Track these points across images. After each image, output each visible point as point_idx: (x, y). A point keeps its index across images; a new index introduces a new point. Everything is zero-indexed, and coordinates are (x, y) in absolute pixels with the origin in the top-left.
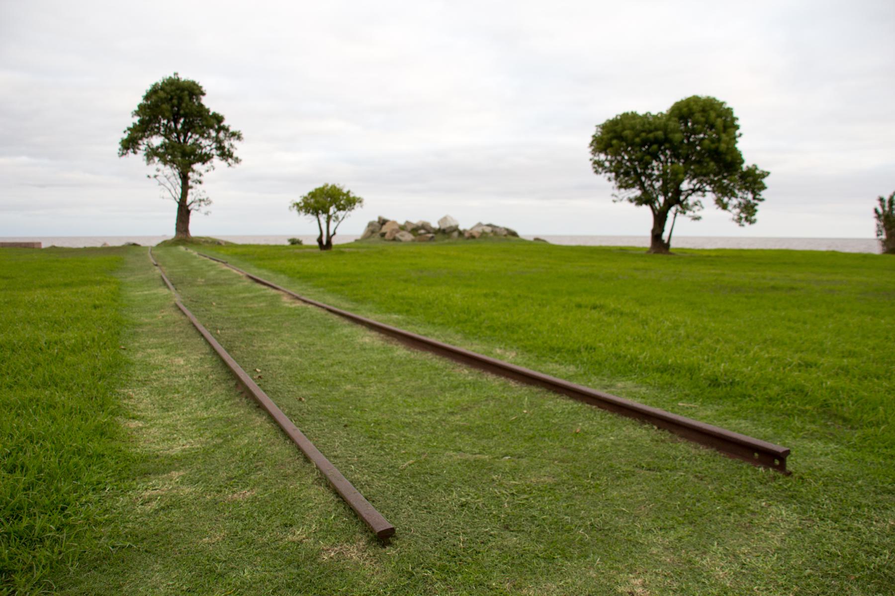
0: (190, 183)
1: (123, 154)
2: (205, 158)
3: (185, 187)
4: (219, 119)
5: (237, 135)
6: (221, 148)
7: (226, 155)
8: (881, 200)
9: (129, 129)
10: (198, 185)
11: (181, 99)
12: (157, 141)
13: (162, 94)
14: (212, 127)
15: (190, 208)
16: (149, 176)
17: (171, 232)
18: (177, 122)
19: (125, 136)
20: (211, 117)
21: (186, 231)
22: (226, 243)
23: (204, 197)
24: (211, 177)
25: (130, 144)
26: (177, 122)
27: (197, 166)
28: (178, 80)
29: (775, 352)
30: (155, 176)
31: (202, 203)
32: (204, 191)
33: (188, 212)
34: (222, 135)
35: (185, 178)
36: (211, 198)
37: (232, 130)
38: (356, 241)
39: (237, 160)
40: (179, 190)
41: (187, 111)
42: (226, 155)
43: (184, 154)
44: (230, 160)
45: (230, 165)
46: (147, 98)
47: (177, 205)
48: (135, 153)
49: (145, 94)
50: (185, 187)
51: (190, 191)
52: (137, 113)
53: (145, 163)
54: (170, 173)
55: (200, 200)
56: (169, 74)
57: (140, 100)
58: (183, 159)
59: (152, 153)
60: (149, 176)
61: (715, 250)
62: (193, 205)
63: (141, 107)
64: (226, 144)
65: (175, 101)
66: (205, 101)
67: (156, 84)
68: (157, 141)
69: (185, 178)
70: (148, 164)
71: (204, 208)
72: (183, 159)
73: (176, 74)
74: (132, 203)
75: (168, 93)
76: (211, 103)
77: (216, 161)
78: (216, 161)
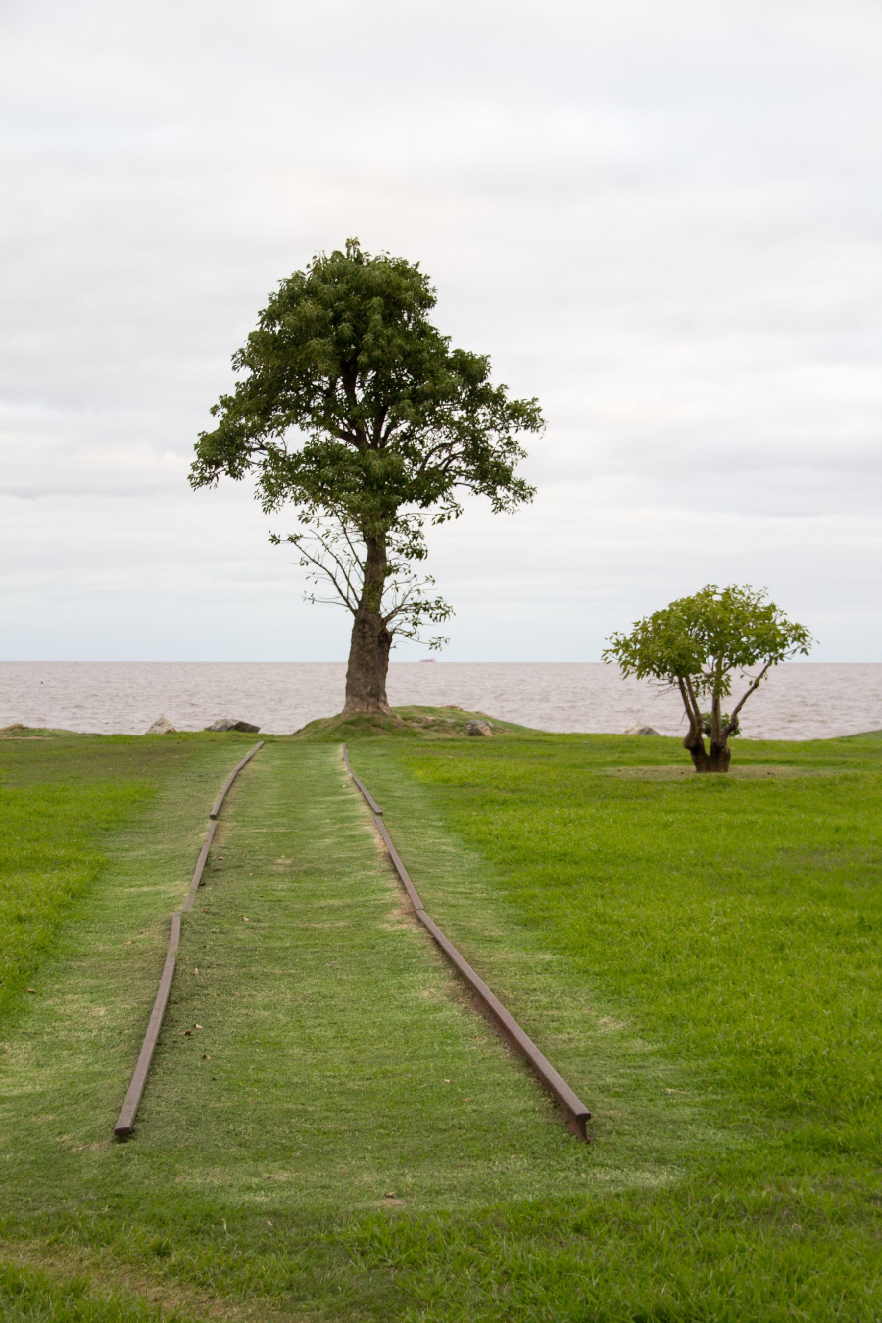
0: (391, 554)
1: (205, 480)
2: (431, 486)
3: (376, 569)
4: (471, 369)
5: (525, 415)
6: (477, 453)
7: (492, 474)
8: (729, 694)
9: (226, 402)
10: (414, 561)
11: (361, 320)
12: (295, 439)
13: (309, 307)
14: (450, 395)
15: (389, 627)
16: (275, 540)
17: (332, 702)
18: (358, 383)
19: (212, 425)
20: (450, 365)
21: (378, 693)
22: (499, 727)
23: (429, 596)
24: (455, 541)
25: (221, 452)
26: (358, 383)
27: (405, 510)
28: (359, 260)
29: (778, 842)
30: (294, 539)
31: (423, 616)
32: (430, 579)
33: (385, 639)
34: (483, 413)
35: (376, 545)
36: (447, 601)
37: (510, 397)
38: (209, 729)
39: (522, 492)
40: (358, 580)
41: (377, 353)
42: (492, 474)
43: (372, 484)
44: (501, 492)
45: (500, 506)
46: (270, 316)
47: (351, 619)
48: (234, 473)
49: (266, 305)
50: (376, 569)
51: (388, 581)
52: (245, 359)
53: (259, 504)
54: (331, 536)
55: (418, 607)
56: (330, 244)
57: (254, 324)
58: (371, 492)
59: (284, 474)
60: (275, 540)
61: (559, 735)
62: (399, 617)
63: (258, 341)
64: (494, 439)
65: (346, 328)
66: (433, 318)
67: (298, 277)
68: (295, 439)
69: (376, 545)
70: (266, 510)
71: (428, 629)
72: (371, 492)
73: (352, 243)
74: (241, 598)
75: (326, 305)
76: (455, 322)
77: (462, 492)
78: (462, 492)
